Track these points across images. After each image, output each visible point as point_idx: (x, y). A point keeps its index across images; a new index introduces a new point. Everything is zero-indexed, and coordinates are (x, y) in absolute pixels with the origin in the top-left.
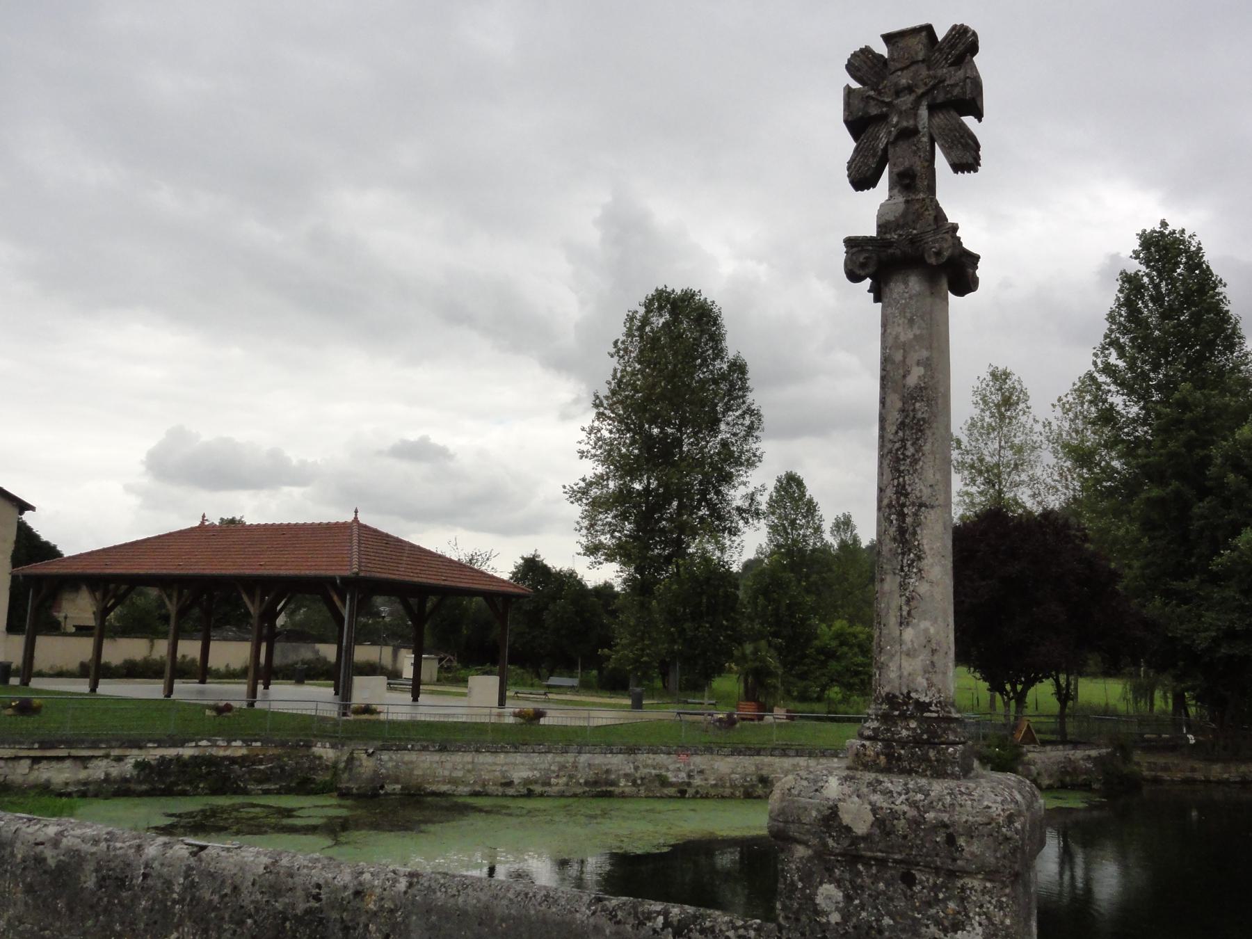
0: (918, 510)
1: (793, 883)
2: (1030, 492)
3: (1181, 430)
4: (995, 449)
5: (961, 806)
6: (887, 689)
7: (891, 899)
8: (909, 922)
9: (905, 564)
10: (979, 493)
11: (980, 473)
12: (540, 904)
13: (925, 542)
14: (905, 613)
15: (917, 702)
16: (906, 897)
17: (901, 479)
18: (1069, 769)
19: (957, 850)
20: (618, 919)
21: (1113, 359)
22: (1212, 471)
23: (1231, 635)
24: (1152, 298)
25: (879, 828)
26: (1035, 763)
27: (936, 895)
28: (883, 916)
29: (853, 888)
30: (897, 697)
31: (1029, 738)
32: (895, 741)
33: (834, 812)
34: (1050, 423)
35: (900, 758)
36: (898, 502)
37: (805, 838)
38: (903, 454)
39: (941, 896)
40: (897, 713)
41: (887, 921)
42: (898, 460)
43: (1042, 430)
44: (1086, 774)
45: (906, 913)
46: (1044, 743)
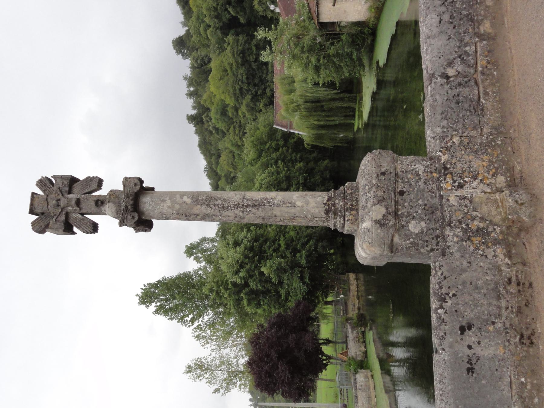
0: (246, 199)
1: (411, 243)
2: (241, 359)
3: (220, 291)
4: (221, 373)
5: (369, 171)
6: (323, 214)
7: (411, 200)
8: (419, 193)
9: (269, 205)
10: (240, 381)
11: (231, 380)
12: (445, 384)
13: (259, 197)
14: (290, 205)
15: (328, 200)
16: (409, 194)
17: (232, 206)
18: (357, 339)
19: (387, 171)
20: (443, 334)
21: (189, 319)
22: (239, 281)
23: (302, 278)
24: (166, 302)
25: (381, 202)
26: (356, 352)
27: (406, 182)
28: (419, 204)
29: (409, 216)
30: (326, 209)
31: (346, 354)
32: (345, 207)
33: (378, 222)
34: (212, 349)
35: (352, 205)
36: (242, 207)
37: (390, 235)
38: (221, 205)
39: (406, 180)
40: (333, 208)
41: (420, 202)
42: (223, 207)
43: (215, 352)
44: (358, 334)
45: (416, 194)
46: (347, 348)
